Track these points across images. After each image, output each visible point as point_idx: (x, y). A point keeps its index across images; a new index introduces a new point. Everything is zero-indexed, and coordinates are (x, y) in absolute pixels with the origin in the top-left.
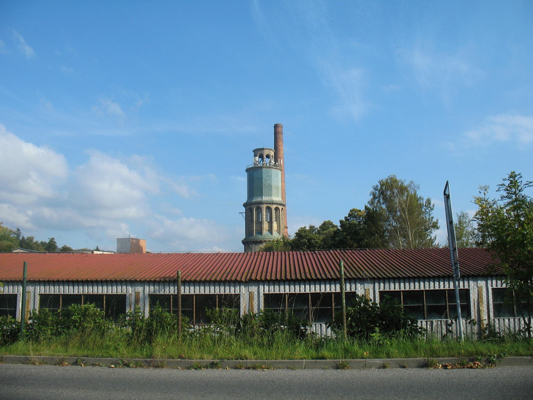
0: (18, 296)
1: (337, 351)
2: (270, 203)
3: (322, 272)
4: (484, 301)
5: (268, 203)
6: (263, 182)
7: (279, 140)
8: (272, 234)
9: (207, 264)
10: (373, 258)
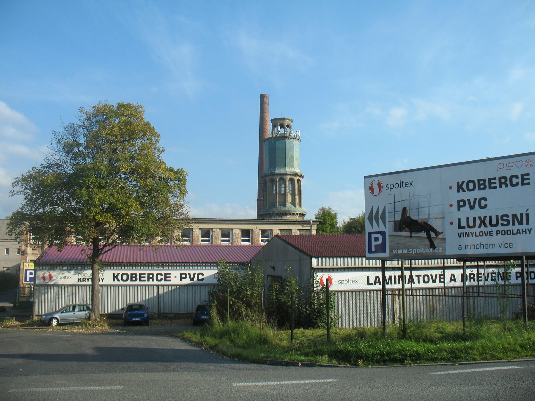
0: (525, 224)
2: (294, 175)
5: (292, 175)
6: (286, 153)
9: (224, 252)
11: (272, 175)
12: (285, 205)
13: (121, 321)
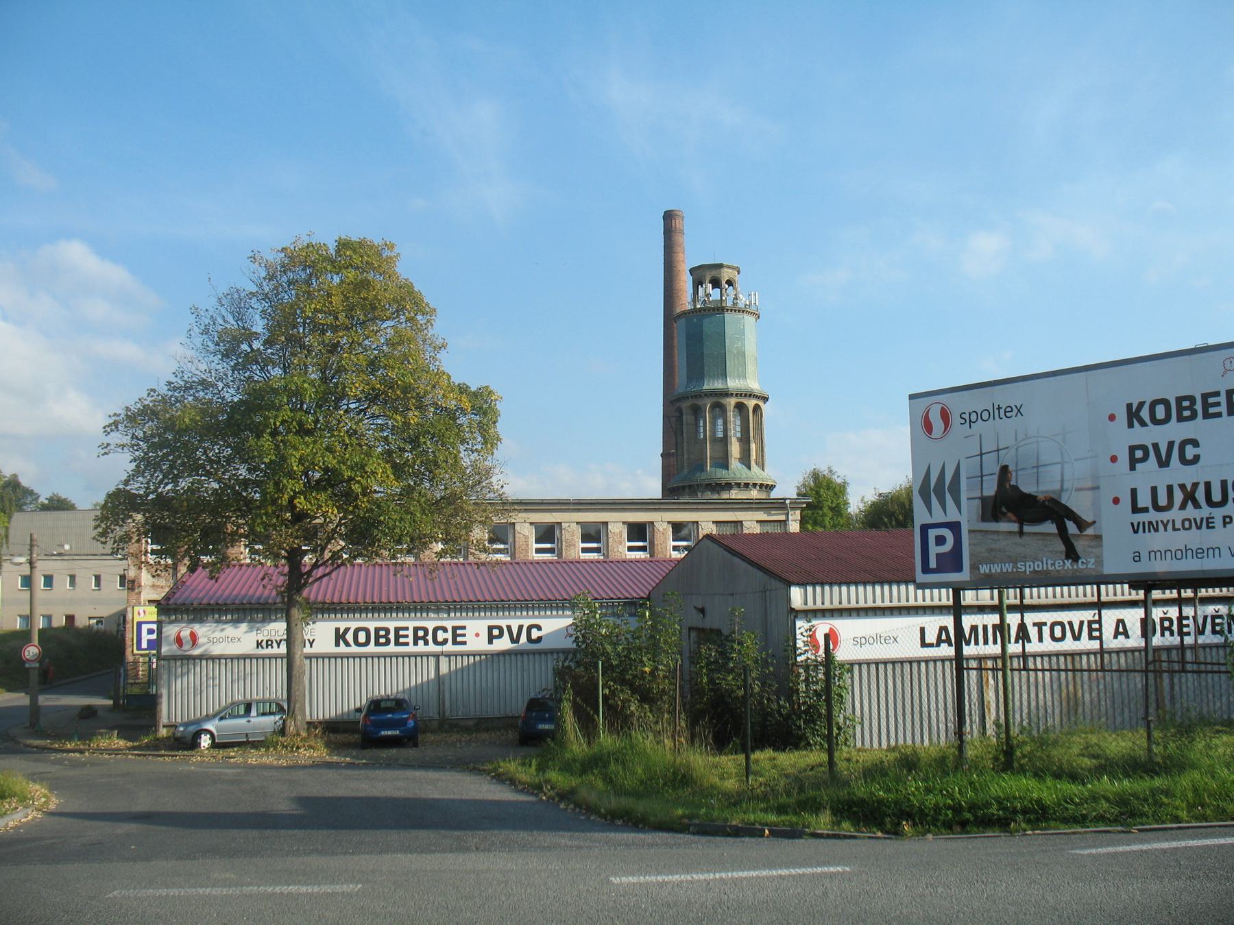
1: (530, 785)
2: (746, 395)
3: (606, 589)
4: (339, 760)
5: (741, 395)
7: (678, 249)
8: (749, 467)
10: (595, 576)
11: (696, 396)
12: (726, 466)
13: (356, 737)
